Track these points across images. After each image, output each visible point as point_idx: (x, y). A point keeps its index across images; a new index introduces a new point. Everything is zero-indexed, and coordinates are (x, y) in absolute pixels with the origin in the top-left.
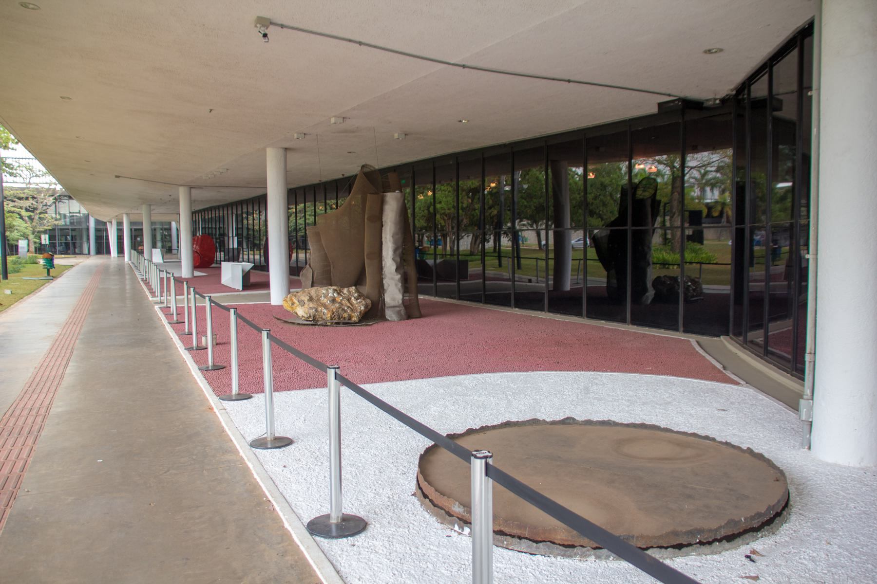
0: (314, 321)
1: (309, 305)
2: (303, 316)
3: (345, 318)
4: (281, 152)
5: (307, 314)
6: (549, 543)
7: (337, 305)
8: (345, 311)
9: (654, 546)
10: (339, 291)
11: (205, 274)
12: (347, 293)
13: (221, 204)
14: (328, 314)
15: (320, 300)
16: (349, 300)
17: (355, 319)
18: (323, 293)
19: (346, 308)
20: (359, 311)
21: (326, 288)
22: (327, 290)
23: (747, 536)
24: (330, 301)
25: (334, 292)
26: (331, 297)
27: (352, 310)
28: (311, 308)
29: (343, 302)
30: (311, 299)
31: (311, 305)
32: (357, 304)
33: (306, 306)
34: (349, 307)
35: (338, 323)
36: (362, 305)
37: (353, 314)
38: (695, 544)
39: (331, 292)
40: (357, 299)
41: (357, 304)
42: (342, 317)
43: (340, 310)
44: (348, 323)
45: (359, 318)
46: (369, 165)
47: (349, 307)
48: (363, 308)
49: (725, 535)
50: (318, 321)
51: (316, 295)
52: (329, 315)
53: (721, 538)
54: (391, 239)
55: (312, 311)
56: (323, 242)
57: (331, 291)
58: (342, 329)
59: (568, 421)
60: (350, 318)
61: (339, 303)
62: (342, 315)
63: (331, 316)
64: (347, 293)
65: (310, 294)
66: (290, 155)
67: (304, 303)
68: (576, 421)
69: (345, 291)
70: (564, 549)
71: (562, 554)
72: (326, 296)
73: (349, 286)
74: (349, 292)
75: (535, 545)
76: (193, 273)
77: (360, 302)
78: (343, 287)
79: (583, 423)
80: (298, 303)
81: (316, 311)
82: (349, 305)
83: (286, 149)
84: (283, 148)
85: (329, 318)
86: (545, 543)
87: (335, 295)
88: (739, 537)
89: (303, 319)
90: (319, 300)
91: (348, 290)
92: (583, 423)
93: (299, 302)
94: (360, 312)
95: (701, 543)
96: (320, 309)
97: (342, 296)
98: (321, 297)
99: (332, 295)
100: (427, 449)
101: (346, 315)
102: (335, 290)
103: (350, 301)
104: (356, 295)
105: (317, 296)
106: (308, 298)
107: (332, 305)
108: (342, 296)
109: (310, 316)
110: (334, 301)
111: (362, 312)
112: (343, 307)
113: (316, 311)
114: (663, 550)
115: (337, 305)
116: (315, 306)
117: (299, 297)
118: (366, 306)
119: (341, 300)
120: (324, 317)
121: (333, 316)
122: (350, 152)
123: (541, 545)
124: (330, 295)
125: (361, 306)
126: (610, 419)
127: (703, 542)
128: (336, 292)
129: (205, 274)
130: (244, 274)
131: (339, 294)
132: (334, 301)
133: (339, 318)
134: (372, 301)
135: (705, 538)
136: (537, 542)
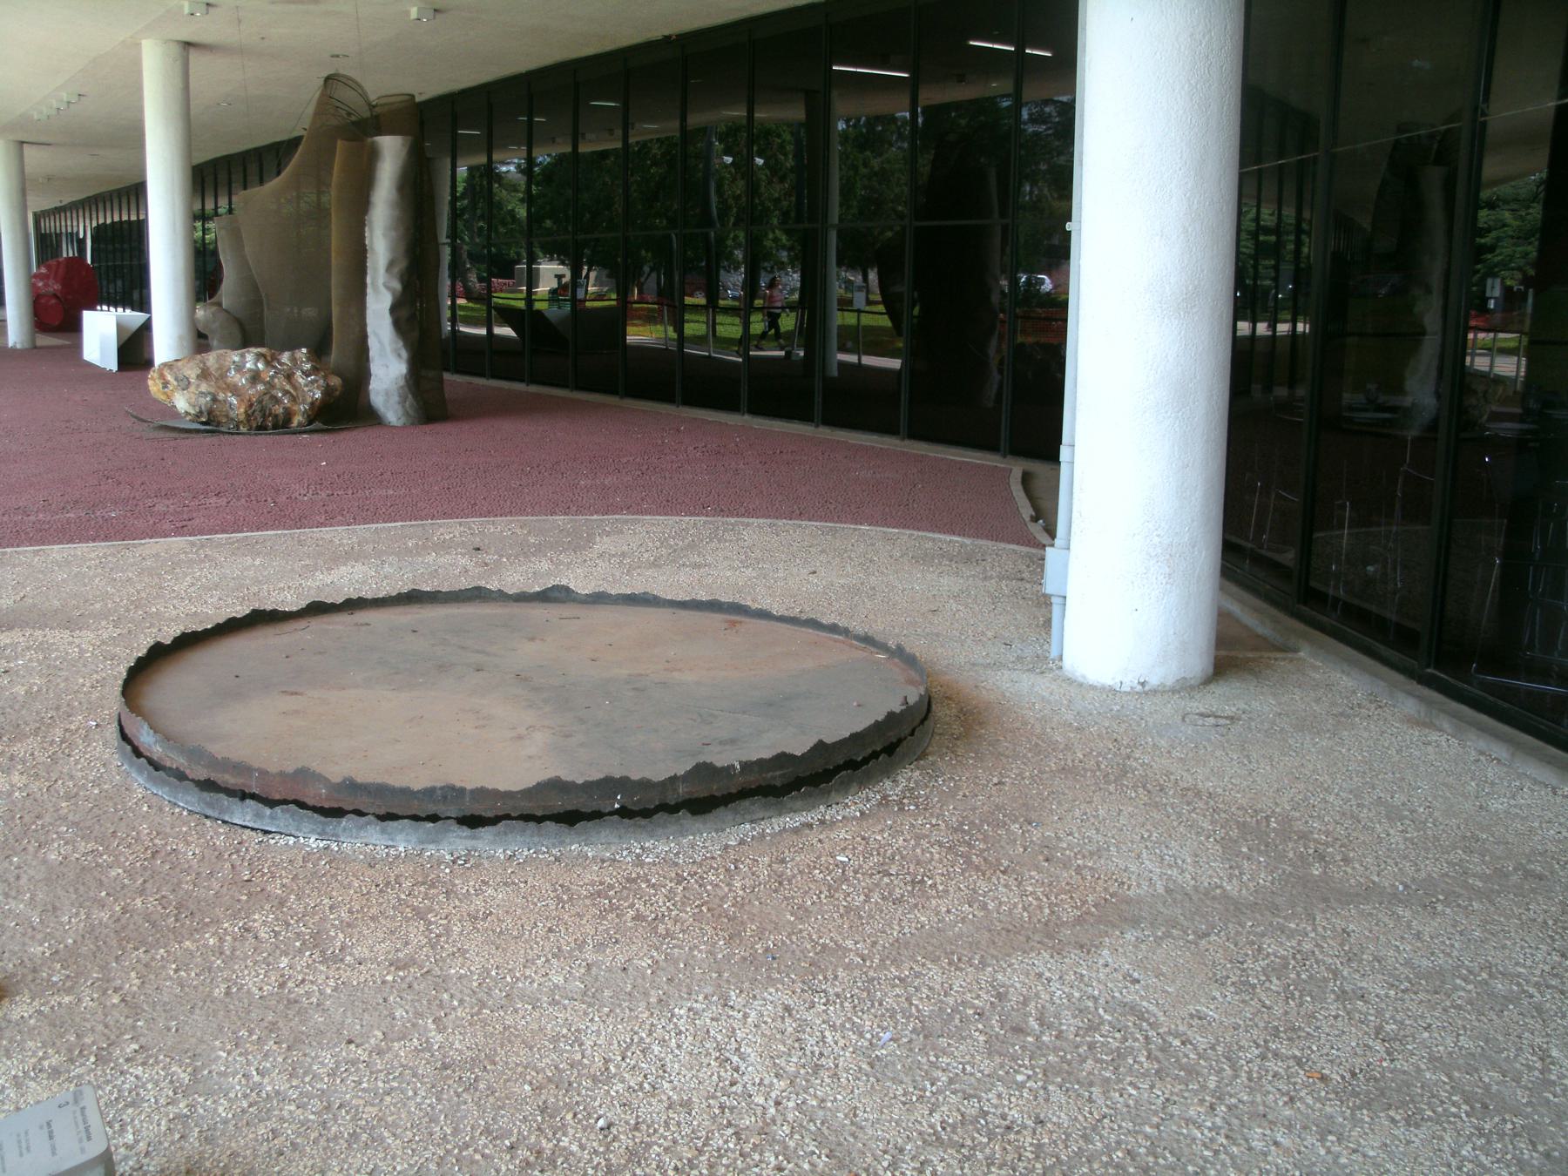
0: (211, 422)
1: (198, 386)
2: (187, 413)
3: (276, 416)
4: (175, 50)
5: (194, 406)
6: (292, 807)
7: (260, 387)
8: (277, 401)
9: (513, 815)
10: (269, 358)
11: (67, 343)
12: (288, 363)
13: (103, 189)
14: (239, 408)
15: (227, 376)
16: (289, 377)
17: (301, 418)
18: (234, 362)
19: (280, 395)
20: (309, 400)
21: (240, 352)
22: (243, 356)
23: (747, 803)
24: (246, 379)
25: (258, 360)
26: (250, 370)
27: (294, 399)
28: (202, 393)
29: (276, 380)
30: (204, 375)
31: (204, 387)
32: (306, 385)
33: (192, 389)
34: (286, 392)
35: (262, 428)
36: (318, 388)
37: (295, 408)
38: (611, 814)
39: (250, 359)
40: (308, 376)
41: (306, 385)
42: (270, 414)
43: (267, 397)
44: (282, 424)
45: (308, 416)
46: (344, 76)
47: (286, 392)
48: (318, 395)
49: (687, 797)
50: (219, 424)
51: (216, 366)
52: (242, 410)
53: (677, 804)
54: (384, 235)
55: (205, 401)
56: (247, 249)
57: (250, 358)
58: (265, 443)
59: (556, 594)
60: (289, 415)
61: (266, 383)
62: (270, 409)
63: (246, 412)
64: (288, 363)
65: (204, 364)
66: (197, 60)
67: (189, 383)
68: (574, 595)
69: (285, 357)
70: (323, 819)
71: (319, 830)
72: (239, 368)
73: (293, 347)
74: (293, 359)
75: (268, 811)
76: (33, 340)
77: (312, 382)
78: (283, 350)
79: (591, 599)
80: (175, 383)
81: (215, 400)
82: (288, 387)
83: (188, 45)
84: (179, 42)
85: (242, 417)
86: (285, 807)
87: (260, 366)
88: (726, 805)
89: (188, 418)
90: (223, 376)
91: (293, 355)
92: (591, 599)
93: (176, 379)
94: (312, 404)
95: (625, 813)
96: (221, 396)
97: (275, 367)
98: (229, 369)
99: (253, 367)
100: (184, 635)
101: (279, 410)
102: (259, 356)
103: (294, 381)
104: (308, 366)
105: (220, 369)
106: (199, 372)
107: (252, 387)
108: (275, 367)
109: (201, 412)
110: (255, 377)
111: (317, 403)
112: (274, 392)
113: (215, 400)
114: (532, 825)
115: (260, 387)
116: (212, 390)
117: (179, 370)
118: (328, 391)
119: (272, 377)
120: (232, 414)
121: (250, 412)
122: (338, 56)
123: (278, 809)
124: (248, 365)
125: (316, 391)
126: (648, 590)
127: (631, 811)
128: (262, 360)
129: (67, 343)
130: (126, 337)
131: (268, 364)
132: (255, 377)
133: (264, 417)
134: (343, 380)
135: (635, 801)
136: (272, 803)
